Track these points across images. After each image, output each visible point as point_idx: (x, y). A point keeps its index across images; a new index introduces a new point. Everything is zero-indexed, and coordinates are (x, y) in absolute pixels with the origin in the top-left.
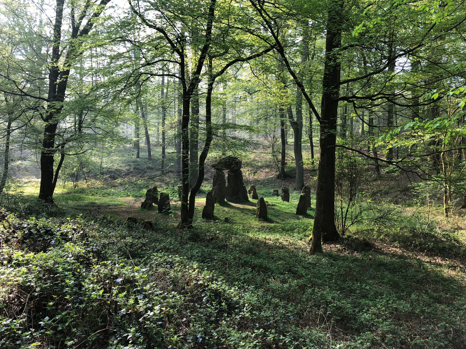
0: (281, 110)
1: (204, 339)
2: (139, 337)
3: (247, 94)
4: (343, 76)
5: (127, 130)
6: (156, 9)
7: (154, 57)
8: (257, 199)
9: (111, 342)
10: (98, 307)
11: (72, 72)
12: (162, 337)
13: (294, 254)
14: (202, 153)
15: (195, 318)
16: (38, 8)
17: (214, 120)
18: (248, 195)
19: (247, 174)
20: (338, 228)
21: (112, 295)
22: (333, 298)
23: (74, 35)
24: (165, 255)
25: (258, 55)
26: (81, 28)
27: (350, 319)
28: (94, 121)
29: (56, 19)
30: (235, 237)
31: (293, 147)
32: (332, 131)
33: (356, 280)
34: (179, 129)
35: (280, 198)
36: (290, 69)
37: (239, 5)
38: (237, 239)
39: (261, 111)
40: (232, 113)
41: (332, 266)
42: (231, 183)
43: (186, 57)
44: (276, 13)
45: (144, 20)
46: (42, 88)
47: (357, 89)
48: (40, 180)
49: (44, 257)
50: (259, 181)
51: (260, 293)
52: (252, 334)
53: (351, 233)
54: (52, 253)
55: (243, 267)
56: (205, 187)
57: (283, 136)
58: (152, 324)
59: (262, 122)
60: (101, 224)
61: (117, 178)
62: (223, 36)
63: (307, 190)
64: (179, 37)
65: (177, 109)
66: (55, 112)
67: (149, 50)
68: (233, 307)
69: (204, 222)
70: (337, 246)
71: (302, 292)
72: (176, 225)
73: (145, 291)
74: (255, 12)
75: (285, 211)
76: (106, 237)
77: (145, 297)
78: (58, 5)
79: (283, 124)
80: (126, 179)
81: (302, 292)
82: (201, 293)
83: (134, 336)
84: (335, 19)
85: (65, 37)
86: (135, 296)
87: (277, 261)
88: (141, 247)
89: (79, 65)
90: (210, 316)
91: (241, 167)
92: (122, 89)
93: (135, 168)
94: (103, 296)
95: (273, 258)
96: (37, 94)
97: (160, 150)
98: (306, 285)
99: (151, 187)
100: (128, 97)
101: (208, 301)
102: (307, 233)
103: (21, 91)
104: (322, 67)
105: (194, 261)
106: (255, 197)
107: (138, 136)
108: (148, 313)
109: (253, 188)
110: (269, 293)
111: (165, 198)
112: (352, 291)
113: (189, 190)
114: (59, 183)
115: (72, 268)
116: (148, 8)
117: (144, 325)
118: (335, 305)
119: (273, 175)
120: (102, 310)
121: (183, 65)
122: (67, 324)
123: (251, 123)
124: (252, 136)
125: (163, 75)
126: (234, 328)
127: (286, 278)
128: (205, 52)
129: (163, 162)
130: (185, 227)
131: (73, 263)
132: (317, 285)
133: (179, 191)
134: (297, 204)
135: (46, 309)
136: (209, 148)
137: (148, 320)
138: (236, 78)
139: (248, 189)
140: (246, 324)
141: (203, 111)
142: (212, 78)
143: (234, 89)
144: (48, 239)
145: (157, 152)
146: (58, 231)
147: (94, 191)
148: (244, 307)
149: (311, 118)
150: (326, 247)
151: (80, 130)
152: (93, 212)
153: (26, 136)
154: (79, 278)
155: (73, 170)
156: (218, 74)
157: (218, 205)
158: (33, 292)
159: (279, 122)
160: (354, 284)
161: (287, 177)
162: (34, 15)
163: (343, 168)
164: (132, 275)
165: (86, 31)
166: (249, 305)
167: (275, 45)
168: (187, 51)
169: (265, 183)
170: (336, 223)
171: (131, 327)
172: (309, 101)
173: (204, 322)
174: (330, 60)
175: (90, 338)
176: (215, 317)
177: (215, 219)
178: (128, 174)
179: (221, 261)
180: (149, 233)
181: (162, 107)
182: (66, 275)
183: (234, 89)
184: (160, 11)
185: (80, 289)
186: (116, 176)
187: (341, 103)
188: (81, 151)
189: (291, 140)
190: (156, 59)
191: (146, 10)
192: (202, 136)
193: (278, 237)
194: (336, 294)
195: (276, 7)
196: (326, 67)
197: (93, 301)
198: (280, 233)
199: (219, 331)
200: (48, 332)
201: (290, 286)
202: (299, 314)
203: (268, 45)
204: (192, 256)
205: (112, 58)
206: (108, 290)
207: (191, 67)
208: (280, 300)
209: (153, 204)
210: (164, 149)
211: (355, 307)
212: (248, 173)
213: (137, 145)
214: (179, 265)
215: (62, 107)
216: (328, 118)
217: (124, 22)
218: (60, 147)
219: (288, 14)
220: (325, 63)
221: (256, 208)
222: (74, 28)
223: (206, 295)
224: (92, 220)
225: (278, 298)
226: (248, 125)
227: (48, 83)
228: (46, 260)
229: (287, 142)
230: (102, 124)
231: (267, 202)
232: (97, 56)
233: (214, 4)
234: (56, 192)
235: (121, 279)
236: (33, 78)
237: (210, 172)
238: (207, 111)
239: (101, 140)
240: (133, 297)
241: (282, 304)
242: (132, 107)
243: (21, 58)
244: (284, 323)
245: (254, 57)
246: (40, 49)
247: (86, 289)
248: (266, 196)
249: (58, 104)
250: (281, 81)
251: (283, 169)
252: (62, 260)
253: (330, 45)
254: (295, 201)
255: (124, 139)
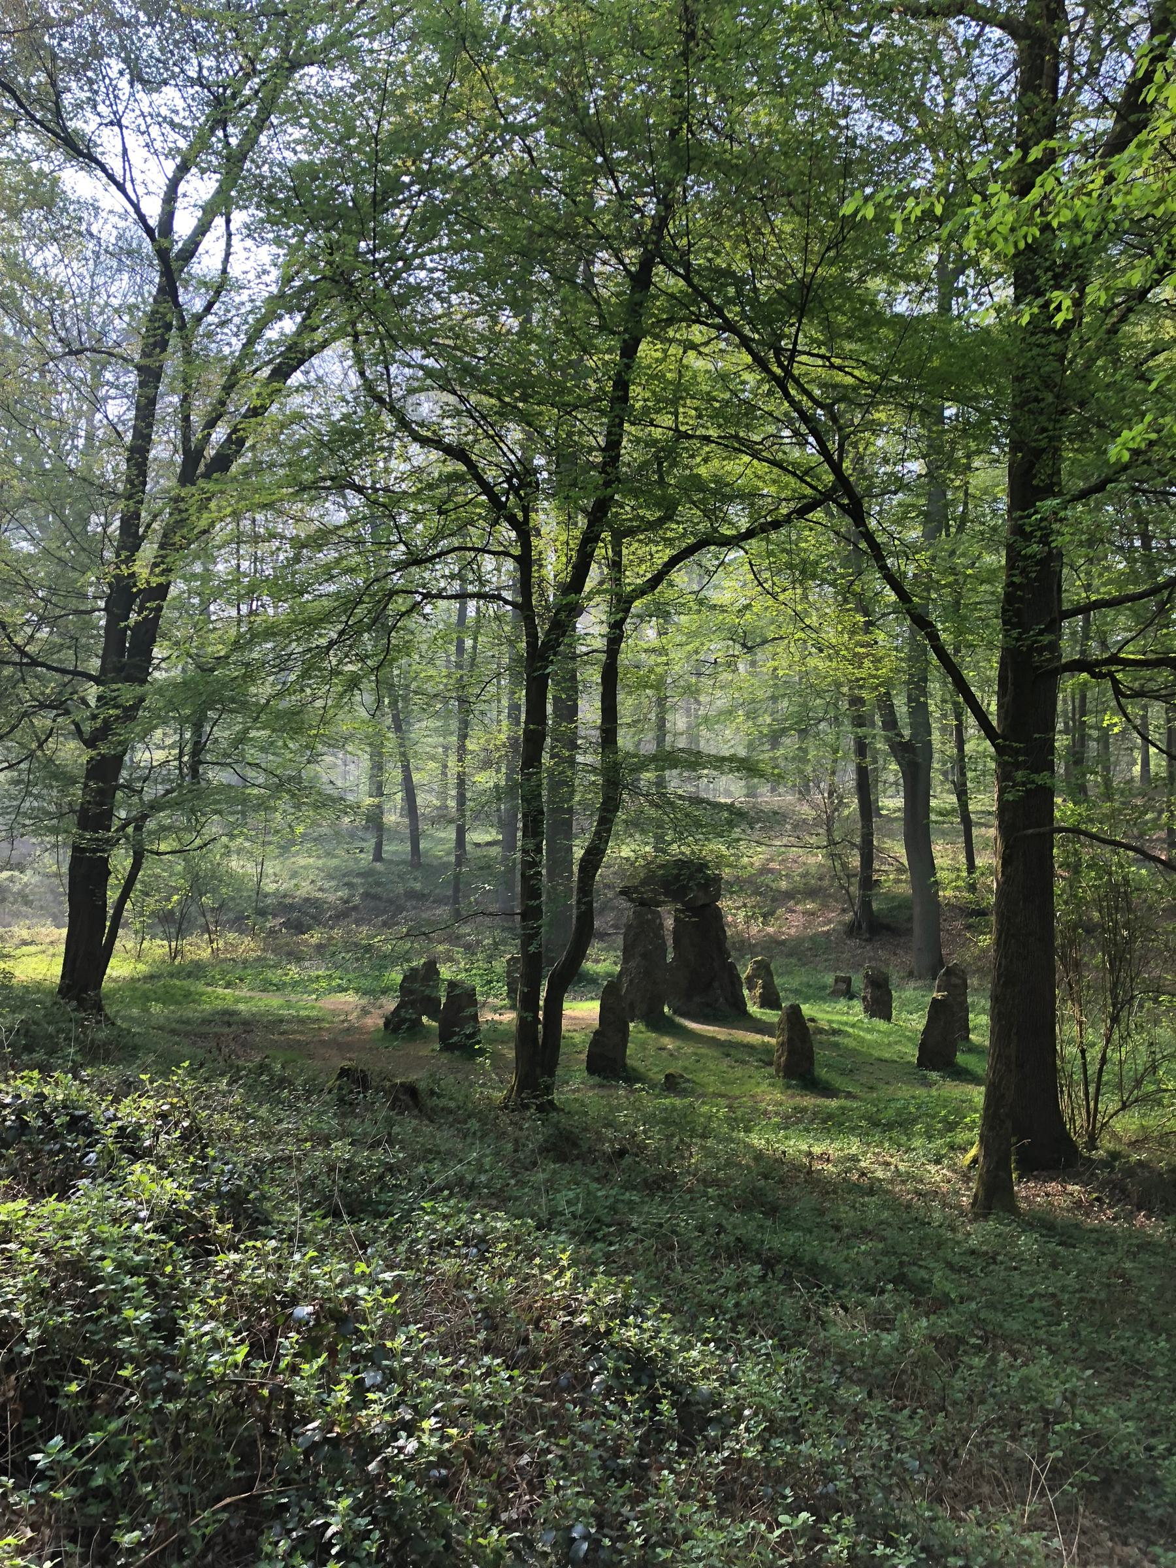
0: (856, 701)
1: (595, 1544)
2: (366, 1535)
3: (738, 649)
4: (1074, 591)
5: (345, 772)
6: (442, 388)
7: (434, 540)
8: (779, 1008)
9: (268, 1548)
10: (228, 1409)
11: (177, 588)
12: (445, 1535)
13: (914, 1214)
14: (588, 852)
15: (562, 1458)
16: (82, 398)
17: (625, 740)
18: (746, 992)
19: (740, 918)
20: (1072, 1120)
21: (276, 1366)
22: (1070, 1397)
23: (187, 477)
24: (460, 1211)
25: (776, 525)
26: (210, 452)
27: (1138, 1481)
28: (241, 739)
29: (135, 427)
30: (703, 1148)
31: (899, 827)
32: (1041, 778)
33: (1152, 1325)
34: (511, 770)
35: (858, 1006)
36: (883, 568)
37: (710, 367)
38: (709, 1153)
39: (785, 703)
40: (688, 710)
41: (1054, 1266)
42: (689, 957)
43: (538, 534)
44: (835, 386)
45: (403, 423)
46: (83, 640)
47: (1120, 628)
48: (64, 931)
49: (59, 1217)
50: (783, 943)
51: (797, 1366)
52: (770, 1529)
53: (1119, 1140)
54: (88, 1194)
55: (730, 1258)
56: (597, 961)
57: (865, 786)
58: (412, 1484)
59: (790, 742)
60: (250, 1088)
61: (310, 928)
62: (660, 464)
63: (955, 980)
64: (515, 474)
65: (505, 702)
66: (118, 717)
67: (418, 517)
68: (697, 1420)
69: (592, 1087)
70: (1070, 1188)
71: (948, 1365)
72: (499, 1095)
73: (391, 1354)
74: (766, 387)
75: (876, 1054)
76: (265, 1136)
77: (391, 1376)
78: (142, 384)
79: (862, 748)
80: (337, 933)
81: (948, 1365)
82: (587, 1358)
83: (347, 1526)
84: (1037, 400)
85: (161, 482)
86: (356, 1373)
87: (854, 1241)
88: (381, 1177)
89: (198, 568)
90: (616, 1453)
91: (718, 897)
92: (332, 643)
93: (366, 896)
94: (246, 1365)
95: (837, 1229)
96: (67, 657)
97: (451, 834)
98: (961, 1340)
99: (418, 962)
100: (350, 667)
101: (608, 1392)
102: (961, 1137)
103: (20, 650)
104: (995, 559)
105: (559, 1233)
106: (769, 1000)
107: (378, 790)
108: (401, 1443)
109: (763, 969)
110: (828, 1363)
111: (463, 999)
112: (1137, 1370)
113: (545, 974)
114: (125, 941)
115: (147, 1262)
116: (416, 384)
117: (384, 1491)
118: (1078, 1426)
119: (830, 922)
120: (242, 1420)
121: (526, 562)
122: (122, 1467)
123: (750, 746)
124: (755, 787)
125: (462, 596)
126: (705, 1507)
127: (889, 1306)
128: (600, 520)
129: (457, 877)
130: (526, 1107)
131: (151, 1243)
132: (1004, 1337)
133: (509, 973)
134: (921, 1027)
135: (55, 1406)
136: (609, 831)
137: (399, 1468)
138: (701, 603)
139: (745, 971)
140: (746, 1487)
141: (589, 711)
142: (622, 604)
143: (692, 635)
144: (77, 1150)
145: (439, 842)
146: (110, 1120)
147: (231, 971)
148: (740, 1418)
149: (960, 729)
150: (1032, 1193)
151: (195, 773)
152: (225, 1046)
153: (28, 793)
154: (168, 1299)
155: (168, 899)
156: (641, 592)
157: (642, 1027)
158: (17, 1343)
159: (849, 742)
160: (1141, 1340)
161: (882, 931)
162: (70, 419)
163: (1080, 902)
164: (346, 1292)
165: (222, 462)
166: (756, 1414)
167: (834, 489)
168: (542, 516)
169: (801, 951)
170: (1064, 1103)
171: (340, 1494)
172: (952, 670)
173: (598, 1474)
174: (1027, 537)
175: (197, 1526)
176: (634, 1454)
177: (631, 1077)
178: (344, 913)
179: (652, 1234)
180: (406, 1126)
181: (459, 699)
182: (126, 1289)
183: (692, 635)
184: (454, 393)
185: (170, 1340)
186: (307, 920)
187: (1069, 684)
188: (198, 842)
189: (892, 802)
190: (443, 544)
191: (411, 391)
192: (586, 789)
193: (854, 1150)
194: (1079, 1379)
195: (832, 366)
196: (1009, 558)
197: (212, 1387)
198: (863, 1135)
199: (645, 1514)
200: (59, 1495)
201: (904, 1339)
202: (942, 1451)
203: (808, 491)
204: (554, 1214)
205: (299, 544)
206: (263, 1347)
207: (553, 565)
208: (870, 1395)
209: (424, 1019)
210: (461, 832)
211: (1154, 1433)
212: (741, 914)
213: (374, 820)
214: (509, 1248)
215: (142, 700)
216: (1024, 733)
217: (341, 432)
218: (130, 830)
219: (877, 388)
220: (1010, 548)
221: (773, 1041)
222: (186, 452)
223: (603, 1367)
224: (222, 1075)
225: (859, 1382)
226: (742, 753)
227: (103, 623)
228: (65, 1228)
229: (879, 809)
230: (268, 753)
231: (812, 1020)
232: (256, 539)
233: (628, 367)
234: (115, 974)
235: (310, 1309)
236: (58, 612)
237: (613, 909)
238: (603, 710)
239: (263, 805)
240: (349, 1376)
241: (876, 1408)
242: (365, 697)
243: (26, 547)
244: (888, 1490)
245: (765, 528)
246: (87, 521)
247: (190, 1342)
248: (806, 1000)
249: (127, 693)
250: (856, 610)
251: (866, 904)
252: (116, 1231)
253: (1027, 487)
254: (912, 1018)
255: (334, 800)
